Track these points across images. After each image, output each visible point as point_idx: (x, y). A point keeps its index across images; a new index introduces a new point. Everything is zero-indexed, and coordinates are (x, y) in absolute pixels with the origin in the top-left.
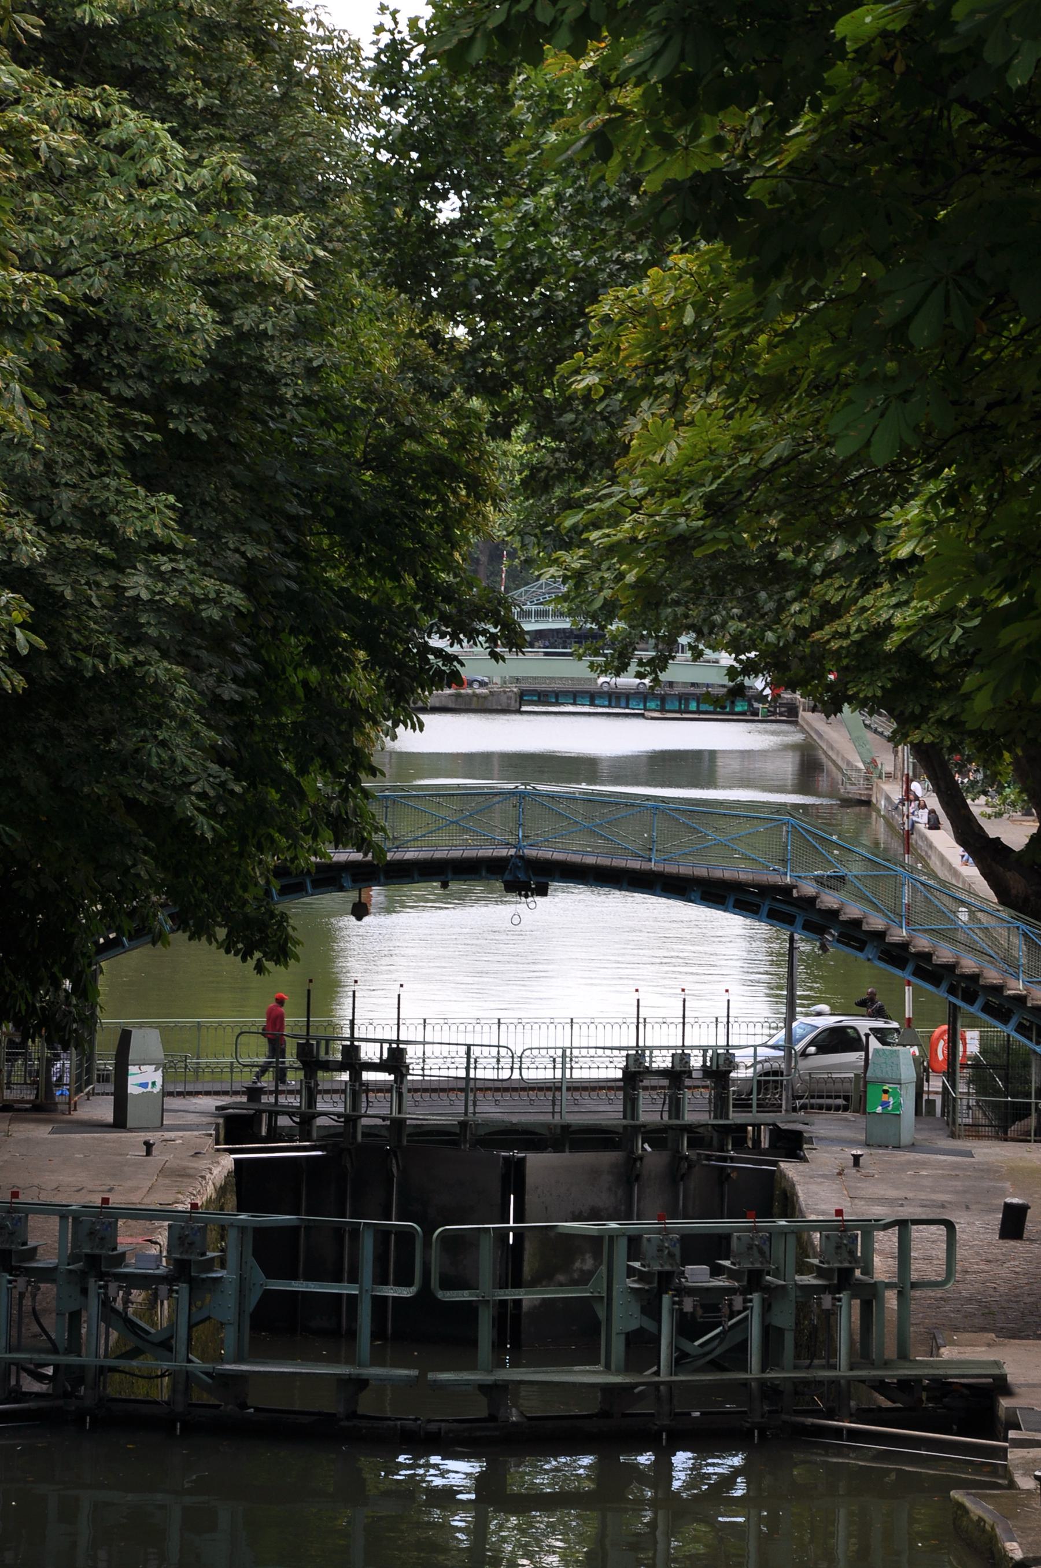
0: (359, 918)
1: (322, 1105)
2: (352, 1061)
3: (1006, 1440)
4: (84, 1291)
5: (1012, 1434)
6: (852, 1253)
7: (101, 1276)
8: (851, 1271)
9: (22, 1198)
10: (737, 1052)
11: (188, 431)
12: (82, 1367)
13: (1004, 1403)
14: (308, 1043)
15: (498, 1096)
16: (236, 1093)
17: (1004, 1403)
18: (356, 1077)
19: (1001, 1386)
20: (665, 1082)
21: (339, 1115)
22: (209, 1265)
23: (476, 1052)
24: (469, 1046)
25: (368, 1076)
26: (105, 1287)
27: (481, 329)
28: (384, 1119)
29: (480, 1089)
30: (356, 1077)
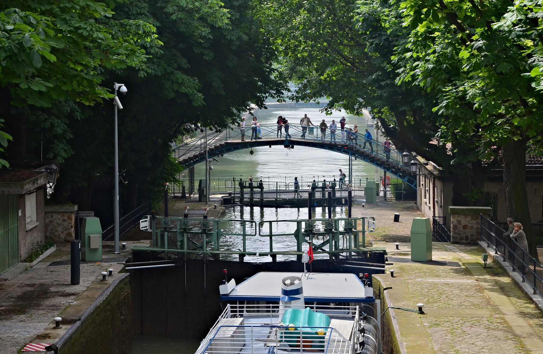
0: (252, 154)
1: (245, 196)
2: (251, 186)
3: (385, 263)
4: (183, 236)
5: (386, 262)
6: (351, 224)
7: (187, 233)
8: (332, 230)
9: (391, 215)
10: (264, 183)
11: (231, 38)
12: (184, 252)
13: (385, 256)
14: (241, 182)
15: (285, 194)
16: (227, 194)
17: (385, 256)
18: (252, 190)
19: (385, 253)
20: (321, 190)
21: (249, 198)
22: (210, 230)
23: (279, 184)
24: (277, 182)
25: (255, 190)
26: (188, 235)
27: (437, 7)
28: (259, 199)
29: (281, 192)
30: (252, 190)
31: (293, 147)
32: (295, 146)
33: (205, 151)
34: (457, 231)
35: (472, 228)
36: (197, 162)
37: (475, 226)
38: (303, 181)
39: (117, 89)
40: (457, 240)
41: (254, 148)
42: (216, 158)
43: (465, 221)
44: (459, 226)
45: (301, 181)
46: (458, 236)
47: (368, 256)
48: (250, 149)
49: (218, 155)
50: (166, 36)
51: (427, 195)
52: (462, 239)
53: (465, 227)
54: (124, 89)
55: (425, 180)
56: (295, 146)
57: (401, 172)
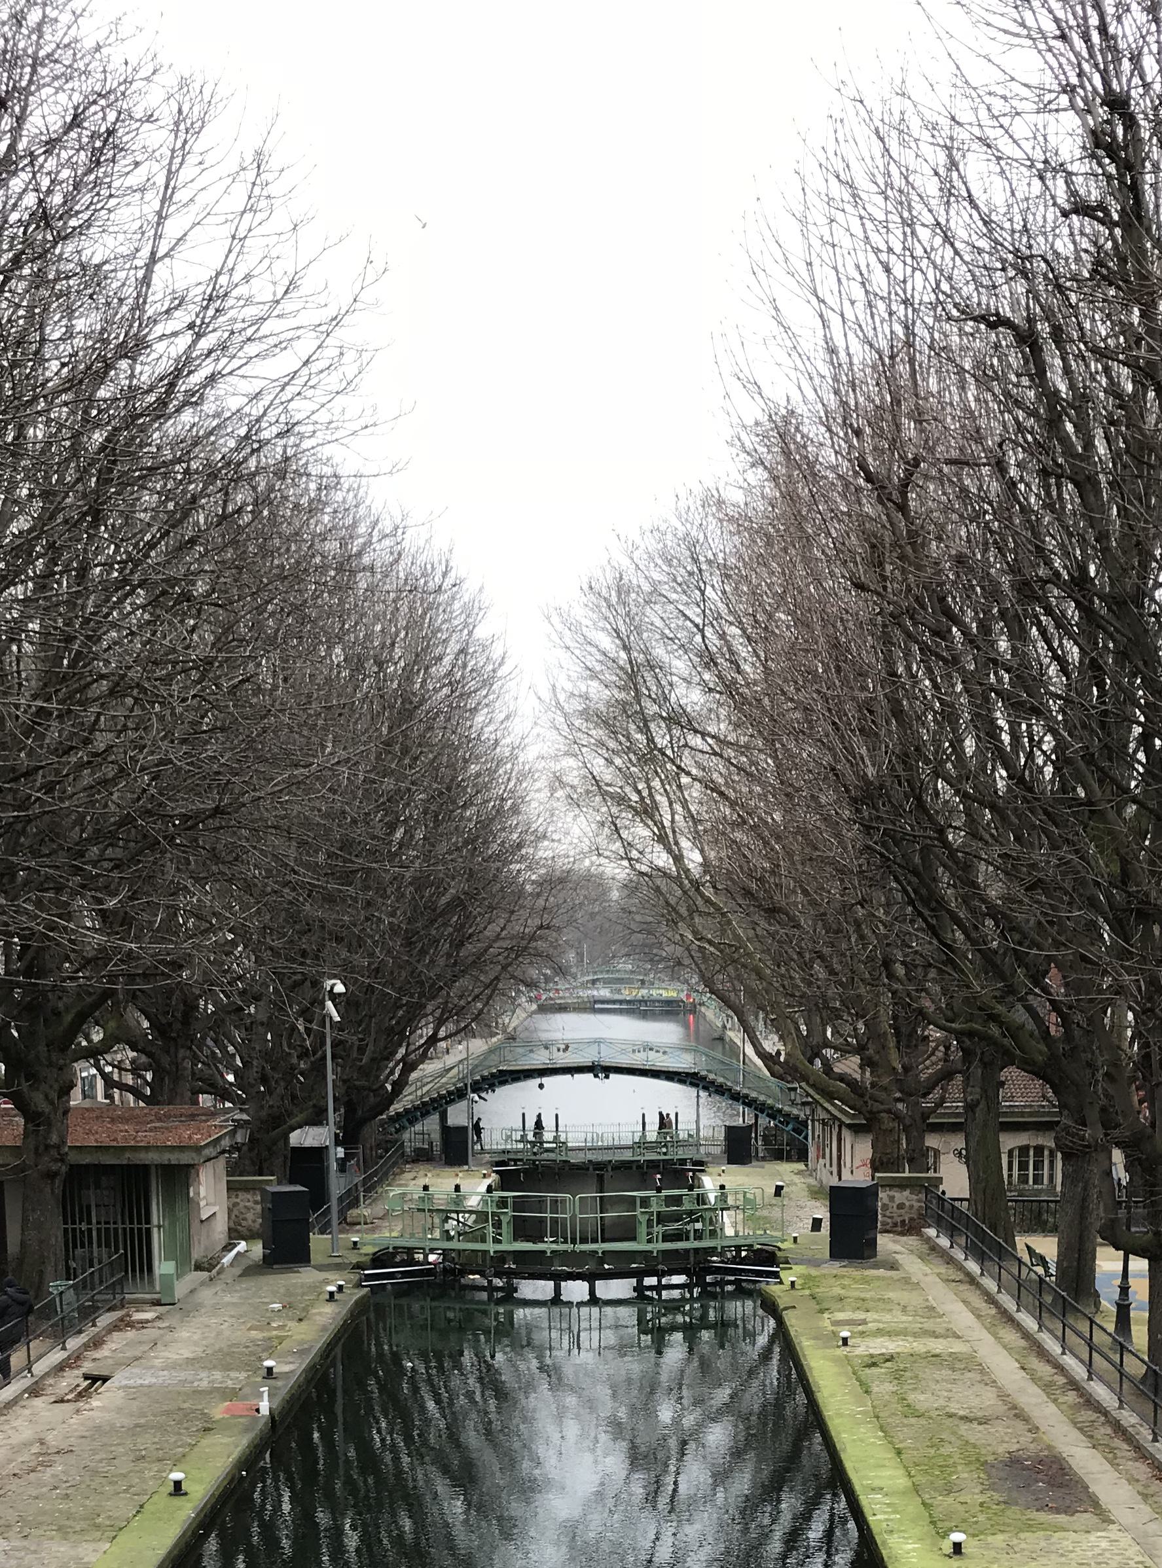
12: (486, 1252)
31: (607, 1077)
32: (611, 1076)
33: (466, 1085)
34: (888, 1213)
35: (911, 1207)
36: (452, 1101)
37: (916, 1205)
38: (595, 1324)
39: (328, 988)
40: (888, 1227)
41: (545, 1080)
42: (483, 1095)
43: (902, 1196)
44: (891, 1204)
45: (595, 1334)
46: (889, 1220)
47: (16, 1034)
48: (538, 1081)
49: (487, 1090)
50: (145, 510)
51: (827, 1151)
52: (895, 1225)
53: (901, 1206)
54: (340, 988)
55: (823, 1130)
56: (611, 1076)
57: (784, 1116)
